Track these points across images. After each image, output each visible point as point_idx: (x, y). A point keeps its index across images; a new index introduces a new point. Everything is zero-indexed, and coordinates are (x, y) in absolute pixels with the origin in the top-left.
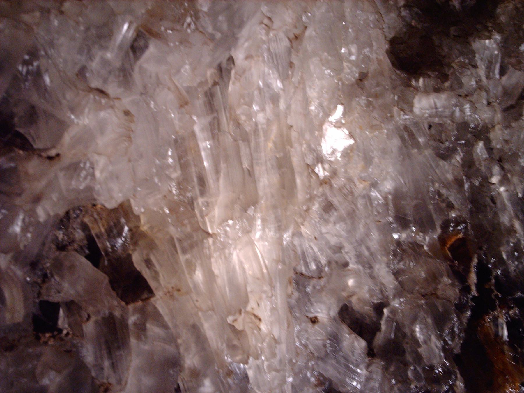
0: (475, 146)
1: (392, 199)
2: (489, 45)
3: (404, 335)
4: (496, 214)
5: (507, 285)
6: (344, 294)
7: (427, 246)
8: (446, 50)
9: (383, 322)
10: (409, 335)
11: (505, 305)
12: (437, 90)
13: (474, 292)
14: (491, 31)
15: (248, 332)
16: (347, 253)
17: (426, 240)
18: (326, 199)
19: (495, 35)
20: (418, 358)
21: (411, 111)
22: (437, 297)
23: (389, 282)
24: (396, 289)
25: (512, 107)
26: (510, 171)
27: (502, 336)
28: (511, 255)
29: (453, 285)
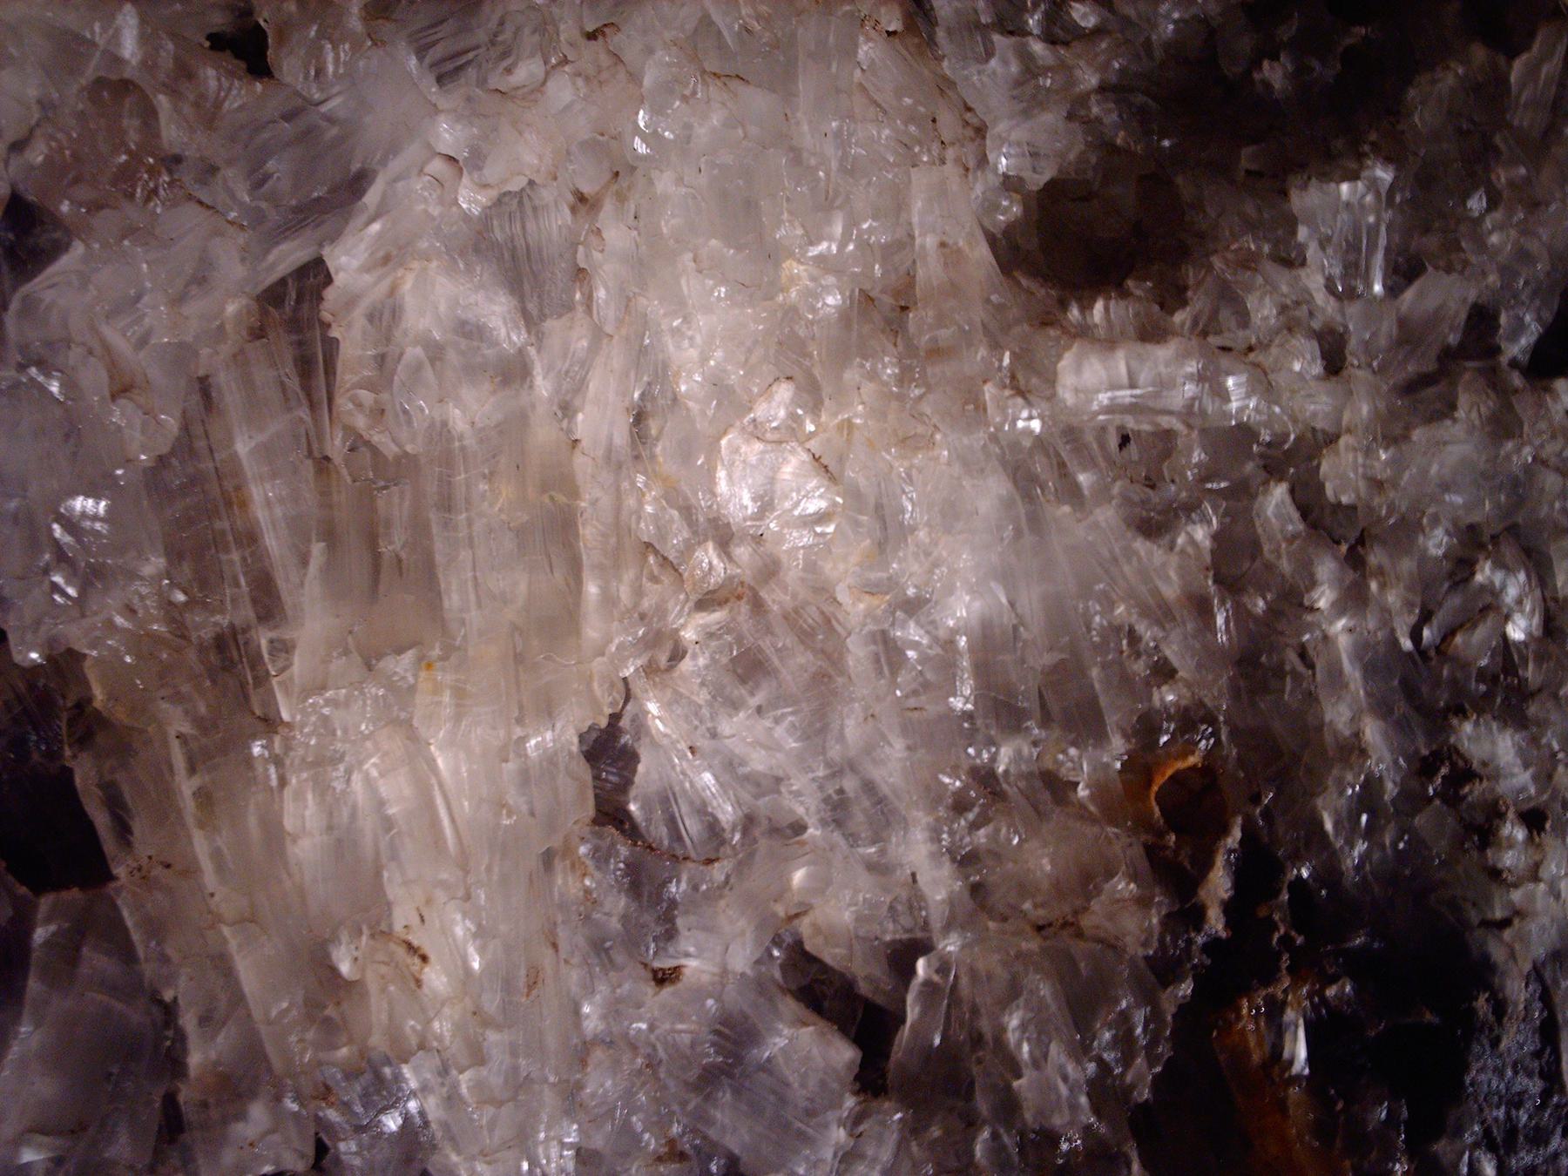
0: (1260, 498)
1: (971, 648)
2: (1349, 200)
3: (977, 1040)
4: (1311, 698)
5: (1325, 913)
6: (780, 910)
7: (1087, 786)
8: (1212, 212)
9: (910, 998)
10: (988, 1036)
11: (1307, 967)
12: (1151, 333)
13: (1216, 922)
14: (1365, 155)
15: (373, 987)
16: (798, 794)
17: (1091, 766)
18: (739, 640)
19: (1373, 168)
20: (1008, 1106)
21: (1052, 397)
22: (1079, 934)
23: (940, 886)
24: (951, 902)
25: (1425, 380)
26: (1380, 572)
27: (1291, 1062)
28: (1347, 823)
29: (1143, 902)
